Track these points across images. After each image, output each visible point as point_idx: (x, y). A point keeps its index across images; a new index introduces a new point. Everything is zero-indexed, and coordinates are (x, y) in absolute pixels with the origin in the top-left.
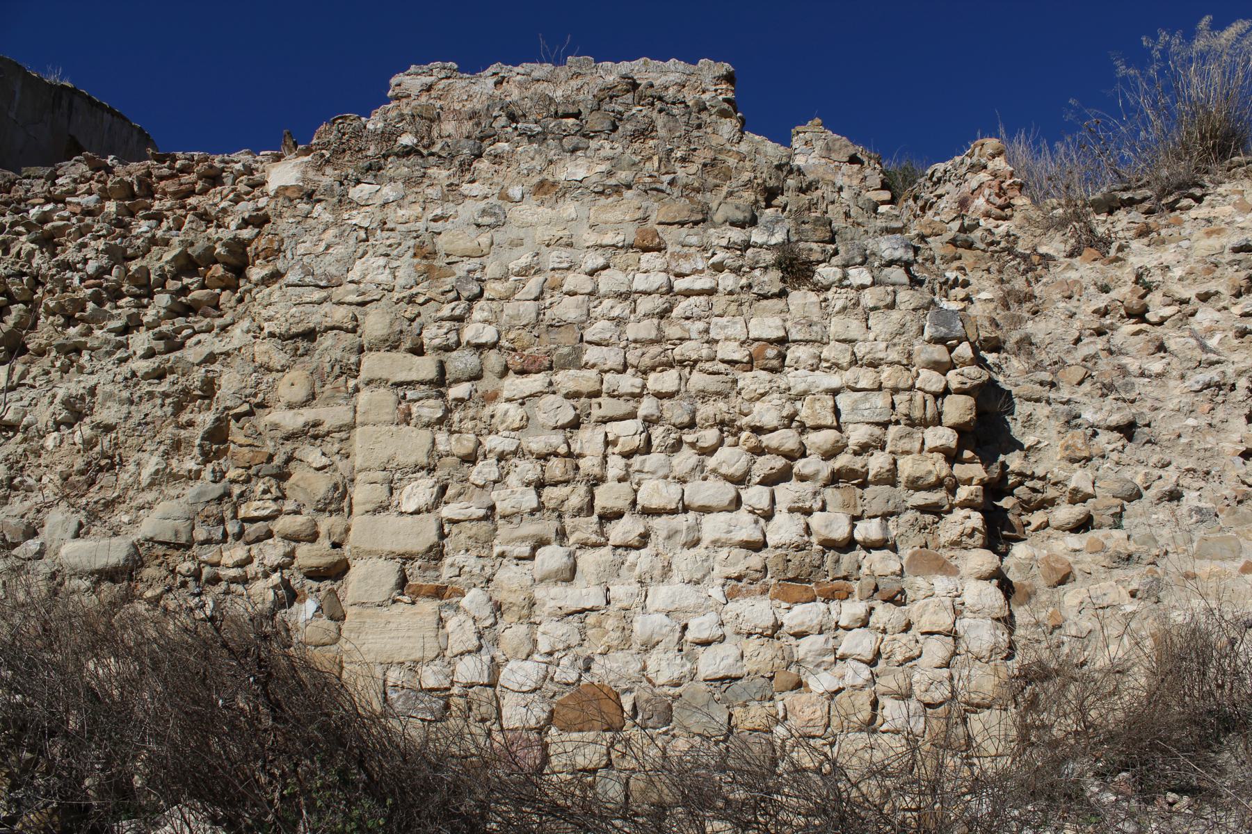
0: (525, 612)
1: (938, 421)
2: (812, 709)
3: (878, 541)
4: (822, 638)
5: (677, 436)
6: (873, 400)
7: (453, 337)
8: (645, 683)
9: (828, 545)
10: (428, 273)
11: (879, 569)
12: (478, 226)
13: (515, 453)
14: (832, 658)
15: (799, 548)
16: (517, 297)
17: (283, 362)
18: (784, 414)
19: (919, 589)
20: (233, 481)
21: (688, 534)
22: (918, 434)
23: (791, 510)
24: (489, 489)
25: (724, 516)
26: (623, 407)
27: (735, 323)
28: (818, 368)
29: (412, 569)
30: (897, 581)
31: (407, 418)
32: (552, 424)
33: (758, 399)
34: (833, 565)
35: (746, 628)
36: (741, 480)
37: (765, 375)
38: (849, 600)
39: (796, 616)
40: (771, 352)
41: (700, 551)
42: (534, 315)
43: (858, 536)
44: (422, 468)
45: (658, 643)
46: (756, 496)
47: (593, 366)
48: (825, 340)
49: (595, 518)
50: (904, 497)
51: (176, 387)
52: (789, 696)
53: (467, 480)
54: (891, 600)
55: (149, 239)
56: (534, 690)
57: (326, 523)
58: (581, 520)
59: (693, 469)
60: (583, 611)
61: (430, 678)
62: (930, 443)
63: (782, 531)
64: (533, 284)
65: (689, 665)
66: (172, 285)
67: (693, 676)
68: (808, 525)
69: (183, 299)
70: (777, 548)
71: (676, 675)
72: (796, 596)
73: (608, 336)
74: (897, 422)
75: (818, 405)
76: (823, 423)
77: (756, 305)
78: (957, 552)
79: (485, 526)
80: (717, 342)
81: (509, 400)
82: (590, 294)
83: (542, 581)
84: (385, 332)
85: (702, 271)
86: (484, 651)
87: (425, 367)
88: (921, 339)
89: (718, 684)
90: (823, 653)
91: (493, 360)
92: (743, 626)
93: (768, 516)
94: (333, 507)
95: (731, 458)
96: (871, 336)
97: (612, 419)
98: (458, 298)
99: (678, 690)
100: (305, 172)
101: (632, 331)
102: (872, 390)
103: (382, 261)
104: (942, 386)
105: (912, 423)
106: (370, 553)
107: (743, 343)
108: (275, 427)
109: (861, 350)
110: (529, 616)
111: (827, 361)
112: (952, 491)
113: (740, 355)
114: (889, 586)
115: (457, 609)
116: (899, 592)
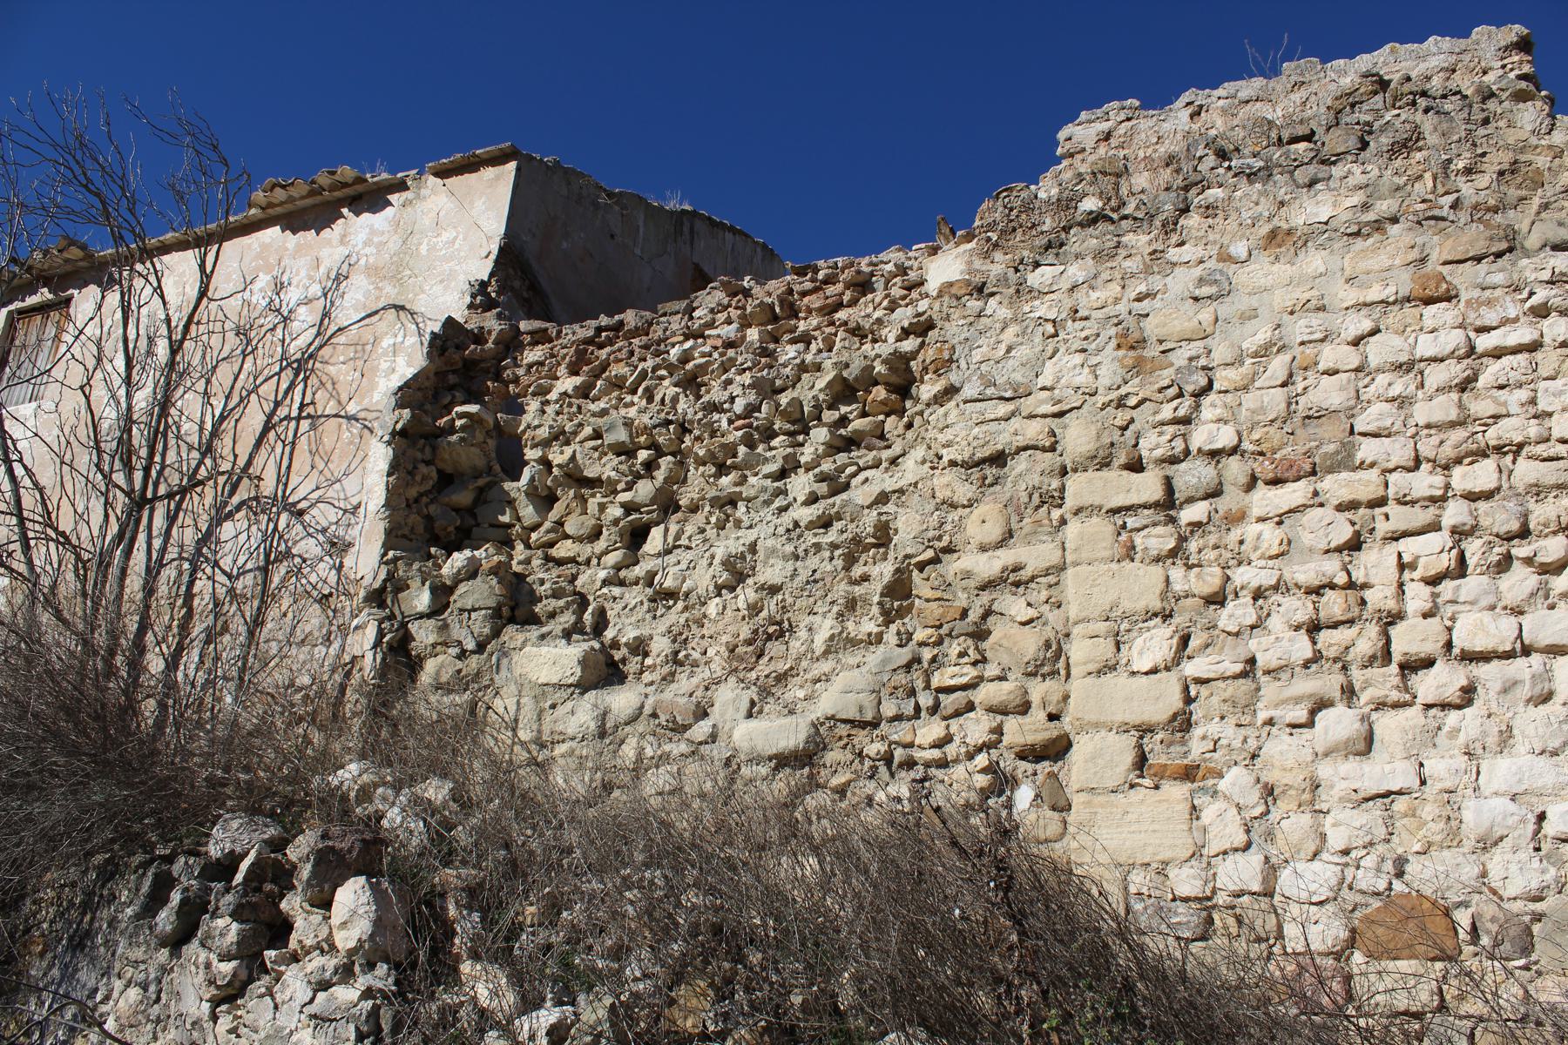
7: (1179, 445)
10: (1138, 368)
12: (1196, 299)
16: (1257, 384)
17: (970, 495)
20: (922, 644)
21: (1534, 685)
29: (1152, 743)
42: (1283, 405)
44: (1155, 615)
45: (1501, 839)
53: (1215, 627)
57: (1038, 690)
64: (1278, 366)
66: (829, 416)
71: (1534, 885)
73: (1388, 423)
79: (1244, 685)
80: (1550, 415)
82: (1357, 370)
83: (1326, 755)
84: (1092, 446)
85: (1516, 320)
87: (1147, 486)
91: (1235, 469)
94: (1046, 669)
97: (1406, 534)
100: (970, 263)
101: (1422, 413)
106: (1097, 726)
108: (967, 575)
110: (1312, 802)
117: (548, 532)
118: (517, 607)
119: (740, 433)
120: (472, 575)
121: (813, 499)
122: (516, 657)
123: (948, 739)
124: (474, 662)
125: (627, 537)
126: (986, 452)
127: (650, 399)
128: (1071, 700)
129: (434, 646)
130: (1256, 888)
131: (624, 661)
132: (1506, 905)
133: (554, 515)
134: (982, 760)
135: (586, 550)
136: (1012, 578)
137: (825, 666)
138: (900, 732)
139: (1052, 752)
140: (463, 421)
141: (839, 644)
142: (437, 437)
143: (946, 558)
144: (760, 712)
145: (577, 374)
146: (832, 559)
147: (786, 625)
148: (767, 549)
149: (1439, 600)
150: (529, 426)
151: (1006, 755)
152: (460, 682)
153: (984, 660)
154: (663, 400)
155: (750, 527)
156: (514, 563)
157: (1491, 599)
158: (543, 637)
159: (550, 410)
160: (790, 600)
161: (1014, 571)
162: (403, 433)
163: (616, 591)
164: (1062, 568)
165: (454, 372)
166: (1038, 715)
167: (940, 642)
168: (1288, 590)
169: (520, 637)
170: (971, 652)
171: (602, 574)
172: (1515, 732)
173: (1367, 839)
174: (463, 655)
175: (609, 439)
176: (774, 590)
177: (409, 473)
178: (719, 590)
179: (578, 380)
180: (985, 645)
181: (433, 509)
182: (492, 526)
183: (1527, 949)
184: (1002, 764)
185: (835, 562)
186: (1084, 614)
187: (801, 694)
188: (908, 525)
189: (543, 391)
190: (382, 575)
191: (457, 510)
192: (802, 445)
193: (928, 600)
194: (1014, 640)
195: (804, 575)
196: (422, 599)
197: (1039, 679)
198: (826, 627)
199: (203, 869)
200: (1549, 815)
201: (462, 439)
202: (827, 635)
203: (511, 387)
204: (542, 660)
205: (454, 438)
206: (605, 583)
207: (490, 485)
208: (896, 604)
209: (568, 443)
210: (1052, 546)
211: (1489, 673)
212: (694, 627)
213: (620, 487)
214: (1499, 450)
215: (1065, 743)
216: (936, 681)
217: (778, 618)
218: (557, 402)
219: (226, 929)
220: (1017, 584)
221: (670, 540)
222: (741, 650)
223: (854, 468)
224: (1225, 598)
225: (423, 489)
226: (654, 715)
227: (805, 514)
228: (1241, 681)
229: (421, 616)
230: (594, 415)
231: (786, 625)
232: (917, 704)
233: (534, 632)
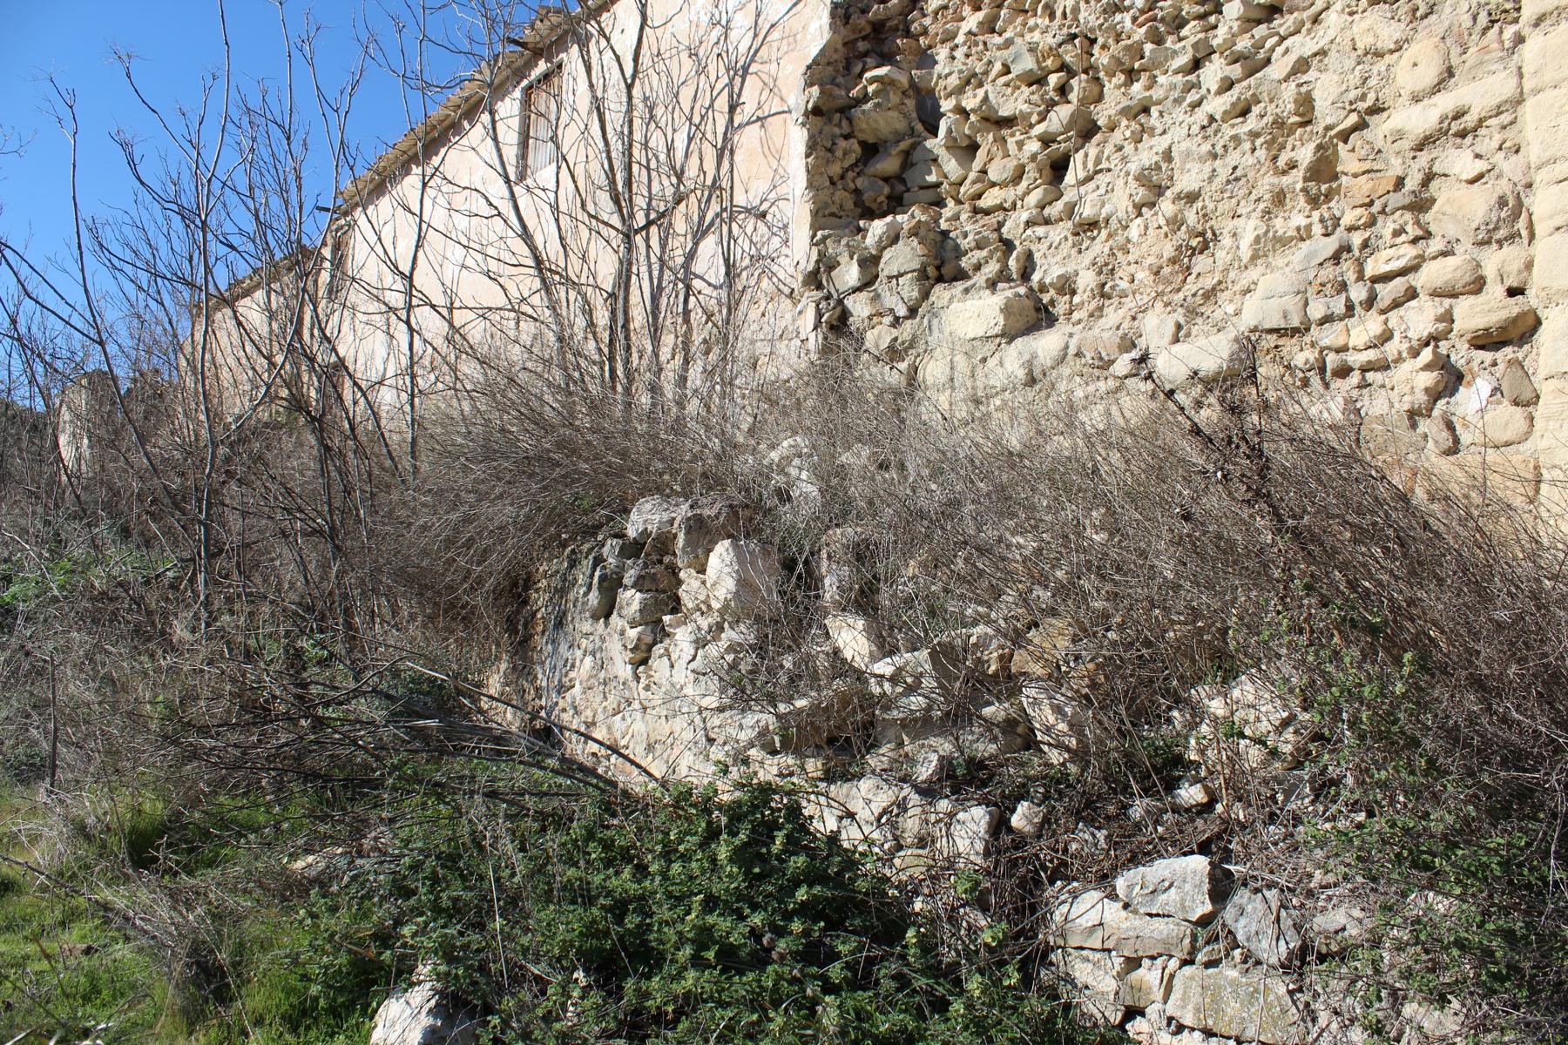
17: (1396, 36)
20: (1350, 229)
57: (1493, 261)
108: (1399, 136)
117: (974, 182)
118: (943, 266)
119: (1144, 29)
120: (895, 240)
121: (1228, 85)
122: (944, 315)
123: (1387, 336)
124: (908, 327)
125: (1047, 171)
127: (1052, 16)
128: (1535, 270)
129: (870, 318)
131: (1052, 302)
133: (977, 164)
134: (1427, 355)
135: (1010, 194)
137: (1253, 274)
138: (1330, 336)
139: (1514, 334)
140: (874, 86)
141: (1268, 246)
142: (851, 107)
143: (1373, 120)
144: (1188, 335)
145: (979, 9)
146: (1254, 150)
147: (1209, 235)
148: (1181, 153)
150: (939, 77)
151: (1458, 346)
152: (894, 353)
153: (1428, 235)
154: (1064, 15)
155: (1164, 132)
156: (942, 221)
158: (967, 291)
159: (959, 54)
160: (1211, 206)
161: (1455, 118)
162: (816, 111)
163: (1040, 231)
164: (1519, 100)
165: (864, 38)
166: (1495, 291)
167: (1372, 222)
169: (947, 295)
170: (1409, 228)
171: (1025, 216)
174: (897, 322)
175: (1016, 70)
176: (1192, 197)
177: (830, 150)
178: (1139, 208)
179: (980, 15)
180: (1428, 217)
181: (860, 182)
182: (922, 188)
184: (1453, 358)
185: (1257, 153)
186: (1548, 155)
187: (1230, 309)
188: (1327, 89)
189: (950, 37)
190: (814, 257)
191: (886, 180)
192: (1216, 27)
193: (1355, 176)
194: (1461, 207)
195: (1224, 174)
196: (849, 274)
197: (1495, 246)
198: (1250, 228)
199: (621, 549)
201: (877, 105)
202: (1252, 238)
203: (921, 40)
204: (967, 315)
205: (869, 106)
206: (1028, 224)
207: (914, 146)
208: (1324, 187)
209: (980, 85)
210: (1504, 74)
212: (1119, 254)
213: (1034, 119)
215: (1531, 321)
216: (1371, 269)
217: (1200, 228)
218: (965, 43)
219: (631, 600)
220: (1462, 134)
221: (1090, 165)
222: (1166, 270)
223: (1276, 39)
225: (846, 164)
226: (1078, 354)
227: (1217, 105)
229: (856, 290)
230: (999, 48)
231: (1209, 235)
232: (1348, 299)
233: (960, 286)
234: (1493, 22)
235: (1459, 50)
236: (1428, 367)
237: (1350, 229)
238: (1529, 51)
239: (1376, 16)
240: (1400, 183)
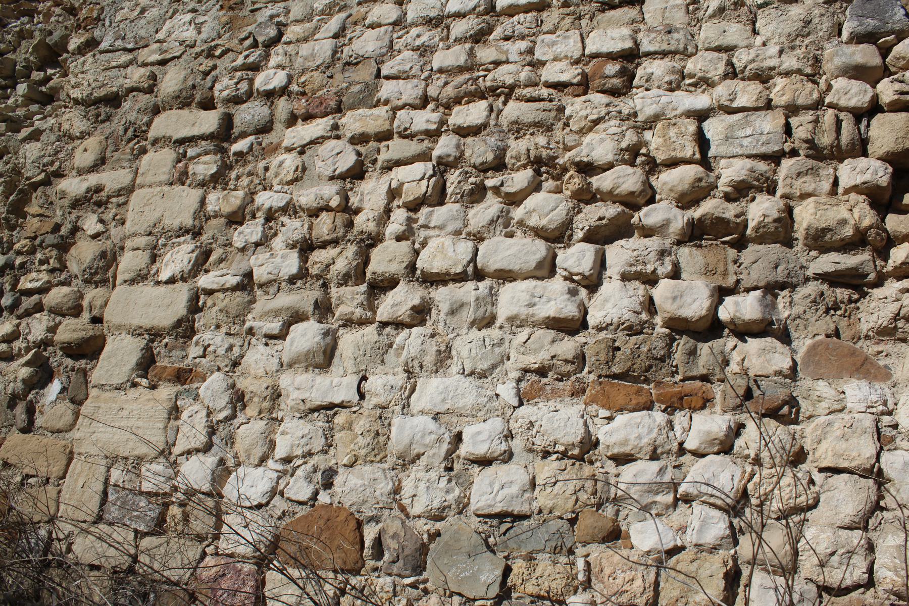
0: (266, 404)
1: (861, 148)
2: (629, 575)
3: (755, 322)
4: (655, 466)
5: (478, 180)
6: (757, 123)
7: (244, 86)
8: (396, 512)
9: (679, 327)
11: (756, 366)
13: (284, 210)
14: (670, 498)
15: (633, 330)
16: (316, 37)
17: (83, 129)
18: (624, 145)
19: (820, 399)
20: (19, 253)
21: (478, 307)
22: (827, 171)
23: (625, 277)
24: (250, 252)
25: (531, 283)
26: (413, 147)
27: (568, 37)
28: (678, 88)
29: (158, 348)
30: (783, 385)
31: (182, 178)
32: (329, 172)
33: (590, 129)
34: (684, 358)
35: (540, 442)
36: (558, 236)
37: (599, 99)
38: (706, 411)
39: (617, 430)
40: (612, 68)
41: (493, 333)
42: (329, 53)
43: (724, 314)
44: (187, 232)
45: (418, 456)
46: (577, 257)
47: (386, 102)
48: (690, 49)
49: (363, 287)
50: (803, 260)
51: (8, 167)
52: (596, 552)
53: (231, 245)
54: (773, 413)
55: (18, 32)
56: (259, 506)
57: (92, 295)
58: (347, 291)
59: (492, 222)
60: (331, 406)
61: (153, 477)
62: (845, 181)
63: (609, 305)
64: (334, 23)
65: (457, 492)
66: (37, 75)
67: (462, 507)
68: (651, 299)
69: (44, 89)
70: (600, 329)
71: (436, 504)
72: (621, 400)
73: (407, 68)
74: (794, 153)
75: (672, 132)
76: (680, 155)
77: (600, 17)
78: (888, 346)
79: (240, 297)
80: (543, 63)
81: (289, 150)
82: (395, 24)
83: (290, 366)
84: (177, 88)
86: (214, 449)
87: (209, 121)
88: (835, 41)
89: (495, 522)
90: (655, 488)
91: (283, 106)
92: (538, 441)
93: (593, 283)
94: (98, 278)
95: (545, 206)
96: (759, 40)
97: (399, 163)
98: (255, 45)
99: (439, 525)
101: (440, 59)
102: (756, 109)
103: (189, 17)
104: (868, 98)
105: (817, 153)
107: (577, 62)
109: (741, 59)
110: (271, 411)
111: (692, 76)
112: (883, 253)
113: (570, 74)
114: (776, 392)
115: (196, 397)
116: (785, 403)
126: (102, 93)
130: (206, 487)
132: (410, 523)
136: (95, 198)
143: (55, 181)
149: (415, 226)
157: (458, 225)
168: (295, 213)
170: (51, 261)
172: (454, 353)
173: (306, 449)
183: (419, 568)
200: (465, 437)
211: (443, 295)
214: (493, 91)
224: (244, 219)
228: (238, 293)
234: (136, 136)
235: (113, 148)
236: (27, 364)
237: (19, 253)
238: (146, 158)
239: (76, 113)
240: (57, 228)
